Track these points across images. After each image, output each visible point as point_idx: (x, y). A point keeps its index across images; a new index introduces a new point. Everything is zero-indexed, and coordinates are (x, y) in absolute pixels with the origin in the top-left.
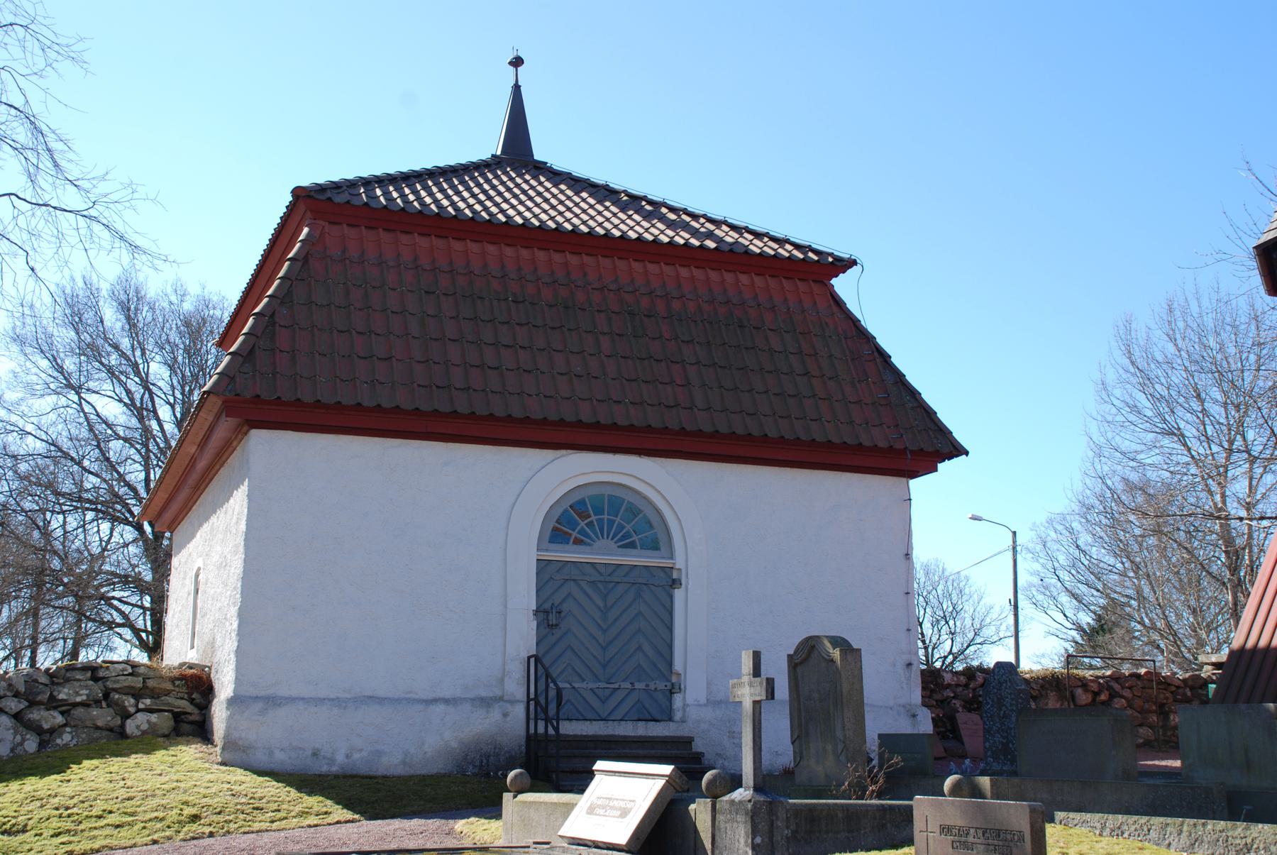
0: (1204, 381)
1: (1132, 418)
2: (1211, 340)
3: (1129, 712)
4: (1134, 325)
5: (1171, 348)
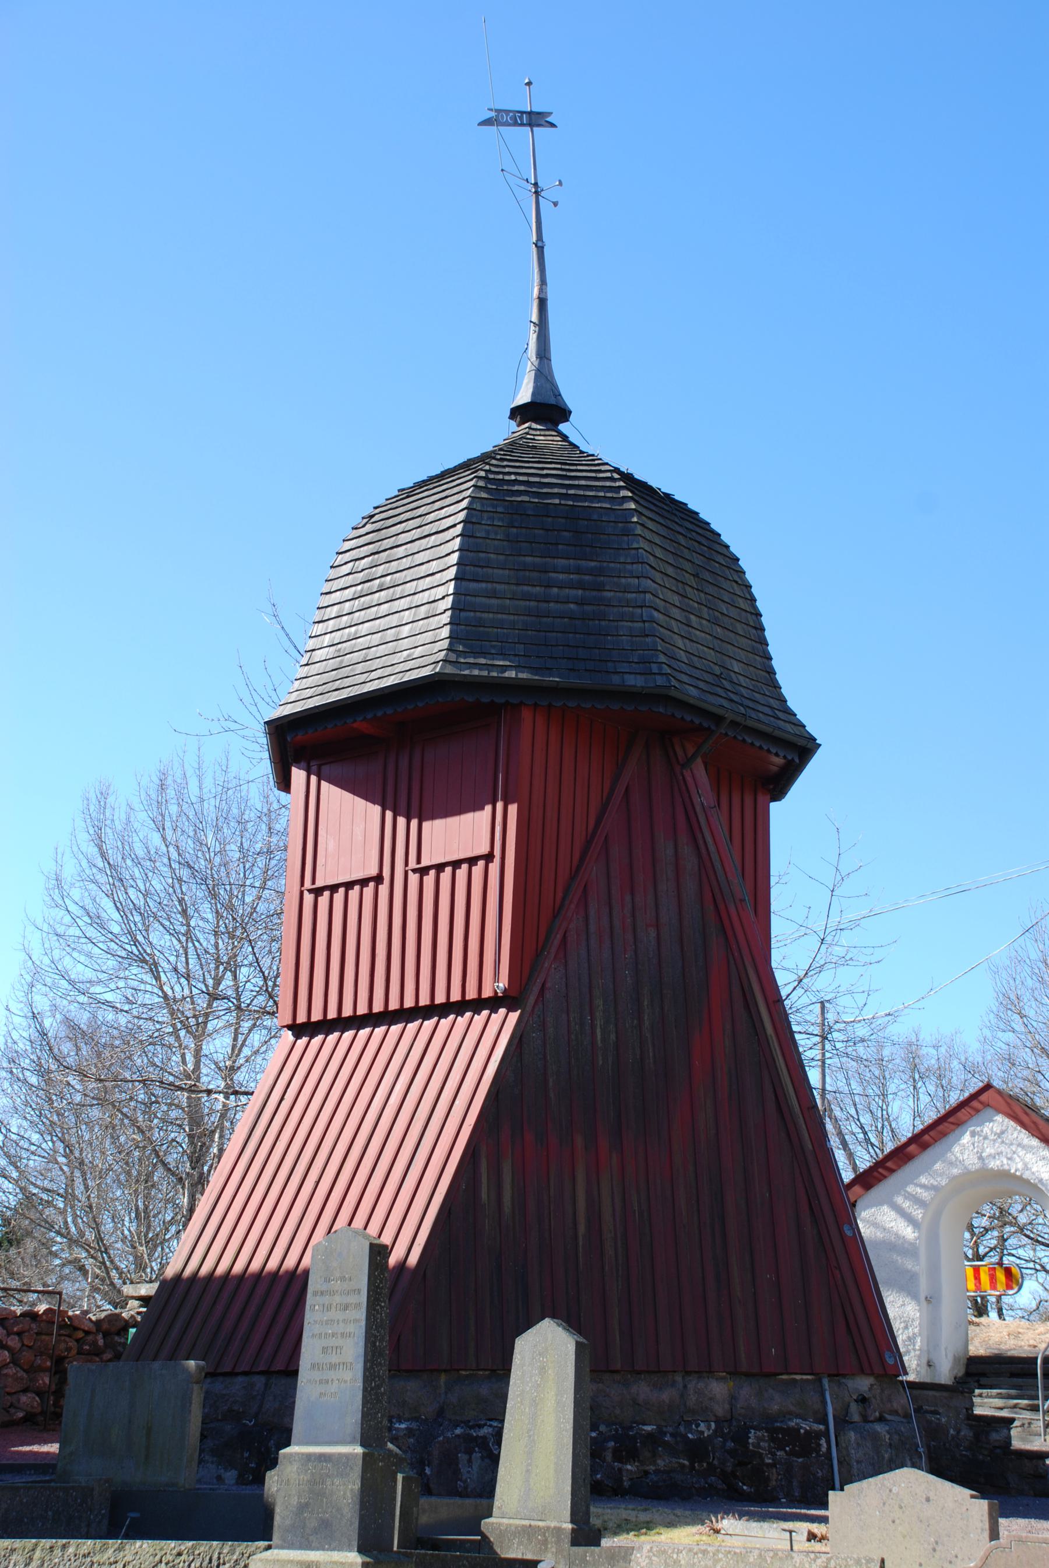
0: (195, 892)
1: (91, 932)
2: (210, 835)
3: (11, 1370)
4: (111, 800)
5: (156, 839)
